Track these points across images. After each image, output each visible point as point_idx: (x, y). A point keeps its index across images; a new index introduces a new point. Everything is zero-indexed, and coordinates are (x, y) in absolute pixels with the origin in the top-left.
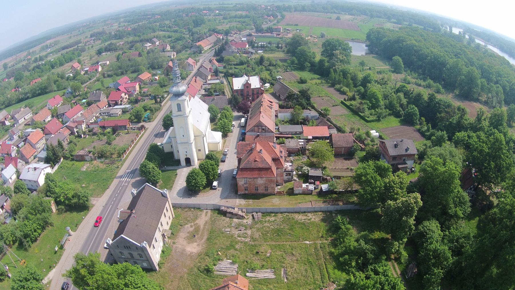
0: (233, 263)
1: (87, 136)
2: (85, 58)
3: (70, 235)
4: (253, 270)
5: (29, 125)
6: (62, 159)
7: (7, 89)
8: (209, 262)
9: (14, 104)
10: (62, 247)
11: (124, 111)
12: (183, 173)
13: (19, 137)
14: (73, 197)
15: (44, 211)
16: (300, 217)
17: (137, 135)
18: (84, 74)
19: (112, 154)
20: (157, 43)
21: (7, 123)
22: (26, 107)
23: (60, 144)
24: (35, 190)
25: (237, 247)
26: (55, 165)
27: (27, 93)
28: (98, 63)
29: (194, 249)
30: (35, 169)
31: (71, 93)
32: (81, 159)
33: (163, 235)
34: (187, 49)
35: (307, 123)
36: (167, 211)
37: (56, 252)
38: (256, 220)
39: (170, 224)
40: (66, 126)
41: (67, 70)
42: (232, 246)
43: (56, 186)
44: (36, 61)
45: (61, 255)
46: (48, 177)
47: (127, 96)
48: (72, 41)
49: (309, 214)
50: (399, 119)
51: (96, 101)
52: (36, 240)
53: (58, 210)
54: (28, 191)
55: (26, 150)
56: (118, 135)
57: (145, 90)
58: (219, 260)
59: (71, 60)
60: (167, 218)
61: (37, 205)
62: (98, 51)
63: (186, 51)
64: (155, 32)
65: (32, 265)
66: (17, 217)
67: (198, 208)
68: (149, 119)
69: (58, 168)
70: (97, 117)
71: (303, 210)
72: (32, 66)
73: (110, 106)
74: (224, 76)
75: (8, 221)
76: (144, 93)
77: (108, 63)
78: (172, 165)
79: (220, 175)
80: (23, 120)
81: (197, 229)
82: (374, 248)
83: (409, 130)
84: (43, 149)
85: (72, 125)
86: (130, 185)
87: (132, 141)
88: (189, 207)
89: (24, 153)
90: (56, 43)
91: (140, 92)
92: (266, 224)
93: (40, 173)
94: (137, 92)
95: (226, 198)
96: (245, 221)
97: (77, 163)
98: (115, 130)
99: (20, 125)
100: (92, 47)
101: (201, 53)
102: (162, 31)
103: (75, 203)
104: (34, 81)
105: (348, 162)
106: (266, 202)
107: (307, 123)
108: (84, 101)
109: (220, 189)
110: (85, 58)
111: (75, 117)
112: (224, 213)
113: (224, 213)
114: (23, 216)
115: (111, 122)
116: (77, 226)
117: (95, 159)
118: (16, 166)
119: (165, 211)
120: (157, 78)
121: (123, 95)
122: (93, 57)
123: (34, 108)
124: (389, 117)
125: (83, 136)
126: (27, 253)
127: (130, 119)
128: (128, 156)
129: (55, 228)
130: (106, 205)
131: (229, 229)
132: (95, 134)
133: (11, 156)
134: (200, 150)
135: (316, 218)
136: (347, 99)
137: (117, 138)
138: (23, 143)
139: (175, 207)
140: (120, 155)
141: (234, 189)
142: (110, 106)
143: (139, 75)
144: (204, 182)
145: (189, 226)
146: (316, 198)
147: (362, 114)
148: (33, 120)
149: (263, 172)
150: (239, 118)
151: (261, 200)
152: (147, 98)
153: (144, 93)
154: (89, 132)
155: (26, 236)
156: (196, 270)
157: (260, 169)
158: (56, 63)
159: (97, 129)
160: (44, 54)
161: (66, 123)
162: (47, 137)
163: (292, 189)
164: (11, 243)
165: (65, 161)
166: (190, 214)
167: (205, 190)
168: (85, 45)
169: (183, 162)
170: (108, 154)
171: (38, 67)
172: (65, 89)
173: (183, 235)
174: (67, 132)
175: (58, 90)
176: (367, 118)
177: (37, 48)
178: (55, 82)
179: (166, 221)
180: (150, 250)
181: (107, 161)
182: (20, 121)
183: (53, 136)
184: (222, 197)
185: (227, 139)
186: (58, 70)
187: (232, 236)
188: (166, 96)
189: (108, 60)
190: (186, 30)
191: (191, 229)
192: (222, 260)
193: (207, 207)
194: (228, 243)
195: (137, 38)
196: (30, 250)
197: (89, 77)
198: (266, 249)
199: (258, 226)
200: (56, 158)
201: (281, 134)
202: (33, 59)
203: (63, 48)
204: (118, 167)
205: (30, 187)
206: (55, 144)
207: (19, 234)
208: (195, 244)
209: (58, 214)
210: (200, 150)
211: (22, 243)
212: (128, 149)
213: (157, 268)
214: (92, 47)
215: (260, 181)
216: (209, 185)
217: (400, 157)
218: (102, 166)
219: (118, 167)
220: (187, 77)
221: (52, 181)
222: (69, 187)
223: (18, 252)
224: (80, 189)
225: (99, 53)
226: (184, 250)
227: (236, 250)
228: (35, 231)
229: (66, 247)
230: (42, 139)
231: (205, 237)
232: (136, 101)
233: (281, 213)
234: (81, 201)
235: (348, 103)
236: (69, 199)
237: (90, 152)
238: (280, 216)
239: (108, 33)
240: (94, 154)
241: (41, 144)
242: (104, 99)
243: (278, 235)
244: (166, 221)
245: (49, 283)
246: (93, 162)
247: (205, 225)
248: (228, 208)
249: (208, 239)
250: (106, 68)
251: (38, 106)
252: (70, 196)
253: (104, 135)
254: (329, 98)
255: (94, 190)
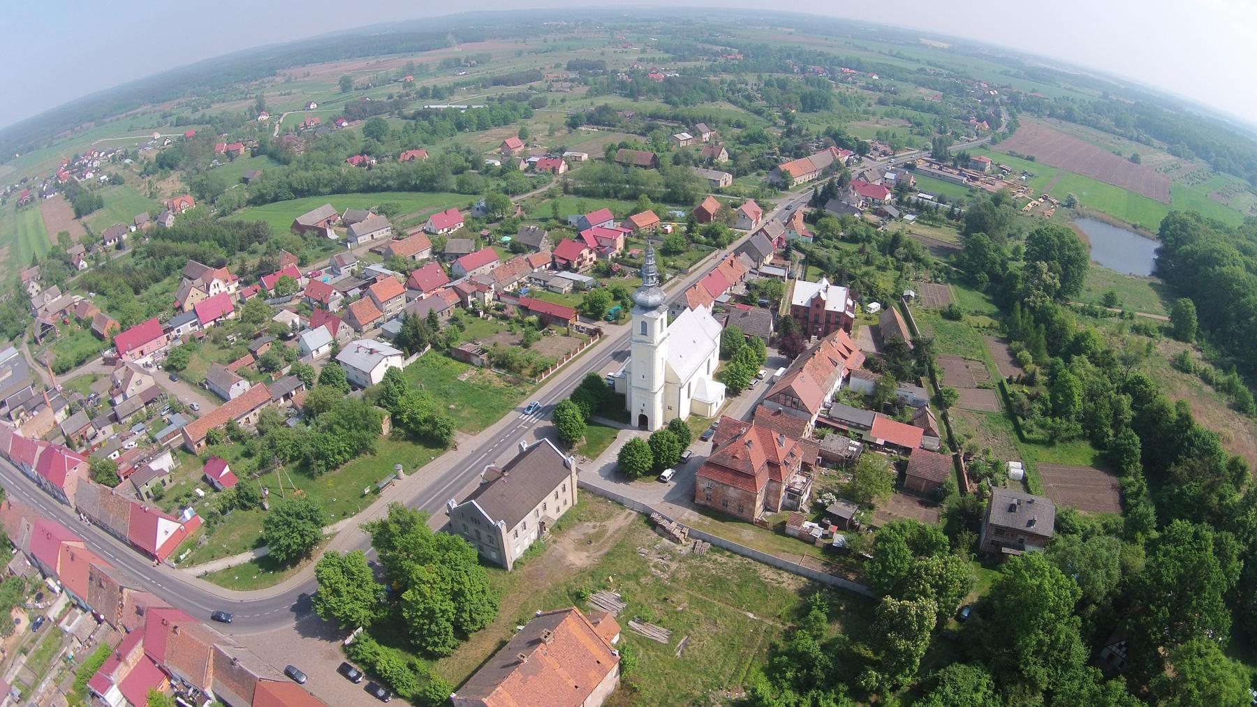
0: (621, 600)
1: (491, 318)
2: (539, 126)
3: (398, 477)
4: (642, 621)
5: (380, 253)
6: (429, 347)
7: (341, 149)
8: (586, 586)
9: (353, 192)
10: (376, 492)
11: (578, 287)
12: (627, 436)
13: (352, 273)
14: (426, 421)
15: (366, 427)
16: (767, 574)
17: (582, 345)
18: (526, 171)
19: (522, 367)
20: (706, 136)
21: (332, 235)
22: (381, 211)
23: (432, 319)
24: (363, 388)
25: (643, 580)
26: (412, 354)
27: (387, 179)
28: (562, 150)
29: (578, 559)
30: (372, 351)
31: (485, 210)
32: (465, 358)
33: (542, 524)
34: (761, 171)
35: (897, 411)
36: (564, 490)
37: (363, 496)
38: (696, 551)
39: (562, 512)
40: (454, 287)
41: (489, 147)
42: (636, 577)
43: (401, 393)
44: (423, 94)
45: (370, 503)
46: (391, 374)
47: (594, 256)
48: (523, 65)
49: (785, 575)
50: (1097, 452)
51: (530, 248)
52: (336, 467)
53: (393, 432)
54: (347, 386)
55: (362, 309)
56: (548, 334)
57: (634, 251)
58: (604, 588)
59: (506, 121)
60: (560, 502)
61: (358, 415)
62: (572, 118)
63: (759, 175)
64: (713, 99)
65: (317, 501)
66: (312, 421)
67: (620, 503)
68: (616, 319)
69: (417, 362)
70: (521, 284)
71: (779, 565)
72: (410, 111)
73: (554, 267)
74: (803, 262)
75: (292, 422)
76: (631, 256)
77: (585, 157)
78: (616, 420)
79: (683, 461)
80: (368, 237)
81: (599, 535)
82: (831, 665)
83: (1105, 481)
84: (397, 316)
85: (467, 288)
86: (531, 432)
87: (568, 354)
88: (605, 496)
89: (357, 312)
90: (481, 60)
91: (623, 254)
92: (709, 565)
93: (381, 362)
94: (617, 251)
95: (673, 502)
96: (679, 547)
97: (455, 363)
98: (545, 322)
99: (359, 246)
100: (563, 101)
101: (785, 188)
102: (730, 101)
103: (426, 433)
104: (410, 153)
105: (923, 510)
106: (730, 531)
107: (897, 411)
108: (507, 238)
109: (673, 484)
110: (539, 126)
111: (478, 271)
112: (653, 525)
113: (653, 525)
114: (324, 423)
115: (548, 303)
116: (416, 467)
117: (489, 367)
118: (334, 331)
119: (559, 488)
120: (669, 228)
121: (585, 252)
122: (558, 130)
123: (399, 219)
124: (1081, 442)
125: (481, 313)
126: (311, 483)
127: (581, 307)
128: (549, 379)
129: (376, 459)
130: (478, 450)
131: (646, 551)
132: (504, 318)
133: (327, 307)
134: (670, 408)
135: (790, 584)
136: (1015, 378)
137: (544, 338)
138: (357, 291)
139: (582, 487)
140: (535, 374)
141: (688, 496)
142: (554, 267)
143: (635, 212)
144: (649, 464)
145: (591, 524)
146: (816, 552)
147: (1020, 420)
148: (389, 251)
149: (741, 479)
150: (776, 364)
151: (726, 524)
152: (633, 270)
153: (631, 256)
154: (498, 309)
155: (320, 456)
156: (564, 589)
157: (737, 473)
158: (469, 121)
159: (512, 310)
160: (444, 81)
161: (457, 278)
162: (412, 294)
163: (784, 523)
164: (288, 458)
165: (434, 353)
166: (603, 507)
167: (647, 479)
168: (549, 89)
169: (635, 421)
170: (516, 364)
171: (425, 115)
172: (475, 193)
173: (575, 534)
174: (454, 299)
175: (459, 192)
176: (1025, 433)
177: (431, 58)
178: (459, 171)
179: (558, 503)
180: (507, 538)
181: (510, 376)
182: (361, 240)
183: (424, 296)
184: (671, 498)
185: (736, 400)
186: (471, 140)
187: (646, 562)
188: (668, 276)
189: (586, 150)
190: (787, 104)
191: (592, 531)
192: (609, 590)
193: (633, 506)
194: (632, 571)
195: (667, 109)
196: (319, 480)
197: (535, 181)
198: (681, 600)
199: (694, 562)
200: (416, 343)
201: (830, 419)
202: (419, 85)
203: (497, 82)
204: (523, 394)
205: (353, 378)
206: (423, 315)
207: (307, 449)
208: (585, 554)
209: (390, 439)
210: (670, 408)
211: (306, 465)
212: (554, 366)
213: (510, 566)
214: (563, 101)
215: (732, 493)
216: (656, 471)
217: (1014, 532)
218: (498, 383)
219: (523, 394)
220: (730, 242)
221: (397, 382)
222: (424, 403)
223: (295, 476)
224: (442, 411)
225: (573, 124)
226: (564, 557)
227: (638, 584)
228: (340, 453)
229: (384, 493)
230: (399, 296)
231: (605, 550)
232: (608, 273)
233: (743, 556)
234: (437, 432)
235: (1009, 389)
236: (417, 422)
237: (484, 351)
238: (738, 559)
239: (609, 69)
240: (489, 357)
241: (397, 306)
242: (546, 248)
243: (715, 587)
244: (558, 503)
245: (333, 536)
246: (484, 370)
247: (615, 532)
248: (663, 518)
249: (608, 554)
250: (577, 169)
251: (408, 218)
252: (420, 417)
253: (521, 323)
254: (983, 367)
255: (468, 420)
